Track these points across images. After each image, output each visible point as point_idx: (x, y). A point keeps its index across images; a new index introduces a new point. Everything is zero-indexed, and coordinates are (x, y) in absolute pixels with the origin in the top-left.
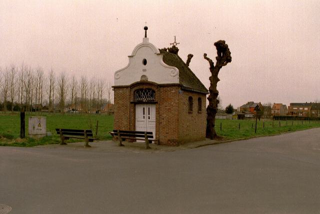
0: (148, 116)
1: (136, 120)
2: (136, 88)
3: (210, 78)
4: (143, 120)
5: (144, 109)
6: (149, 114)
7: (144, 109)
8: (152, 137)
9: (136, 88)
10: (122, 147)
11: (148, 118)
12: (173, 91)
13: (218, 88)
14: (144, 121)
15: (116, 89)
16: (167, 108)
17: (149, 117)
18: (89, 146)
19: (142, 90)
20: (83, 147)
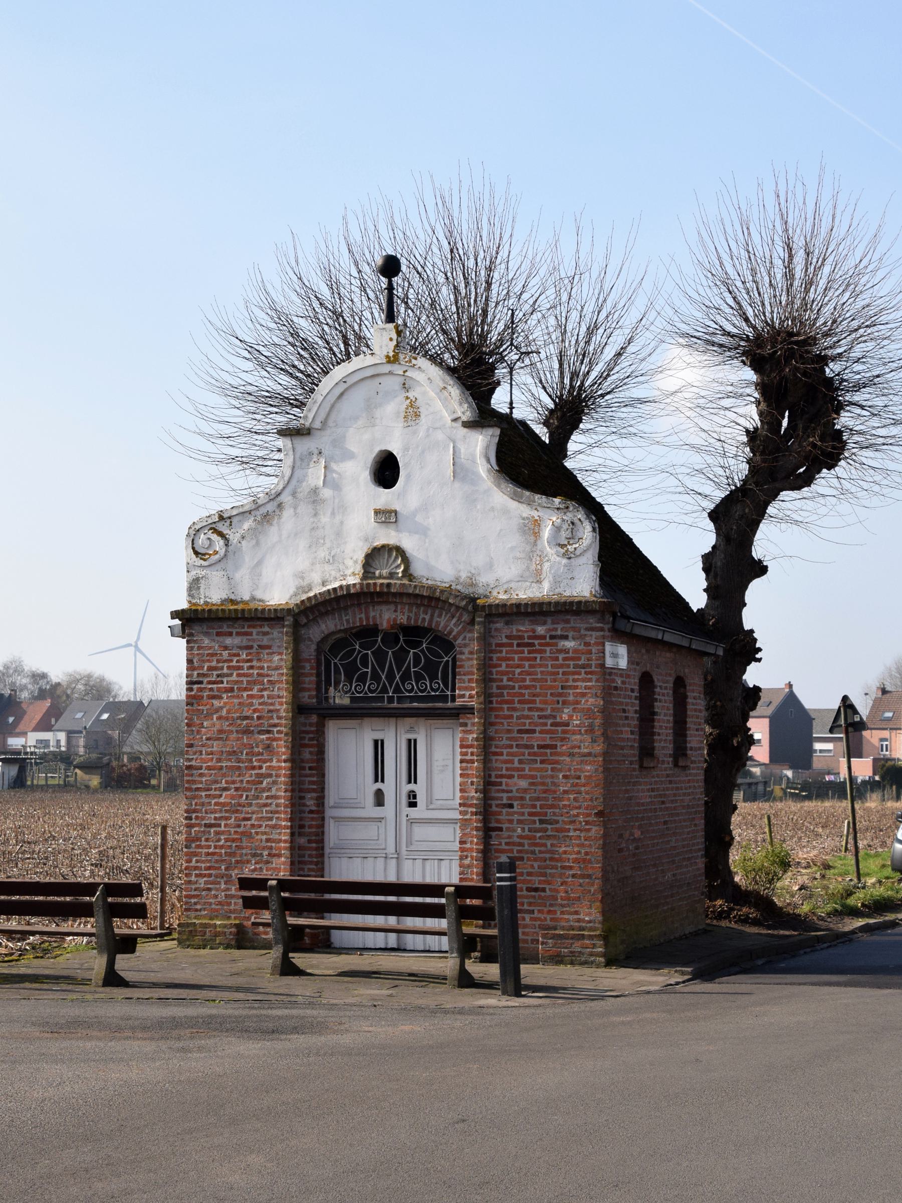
0: (407, 788)
1: (329, 813)
2: (328, 625)
3: (709, 563)
4: (373, 811)
5: (378, 746)
6: (412, 777)
7: (378, 746)
8: (140, 912)
9: (328, 625)
10: (119, 993)
11: (404, 801)
12: (569, 644)
13: (750, 619)
14: (380, 820)
15: (196, 629)
16: (537, 739)
17: (412, 795)
18: (298, 972)
19: (368, 633)
20: (438, 979)
